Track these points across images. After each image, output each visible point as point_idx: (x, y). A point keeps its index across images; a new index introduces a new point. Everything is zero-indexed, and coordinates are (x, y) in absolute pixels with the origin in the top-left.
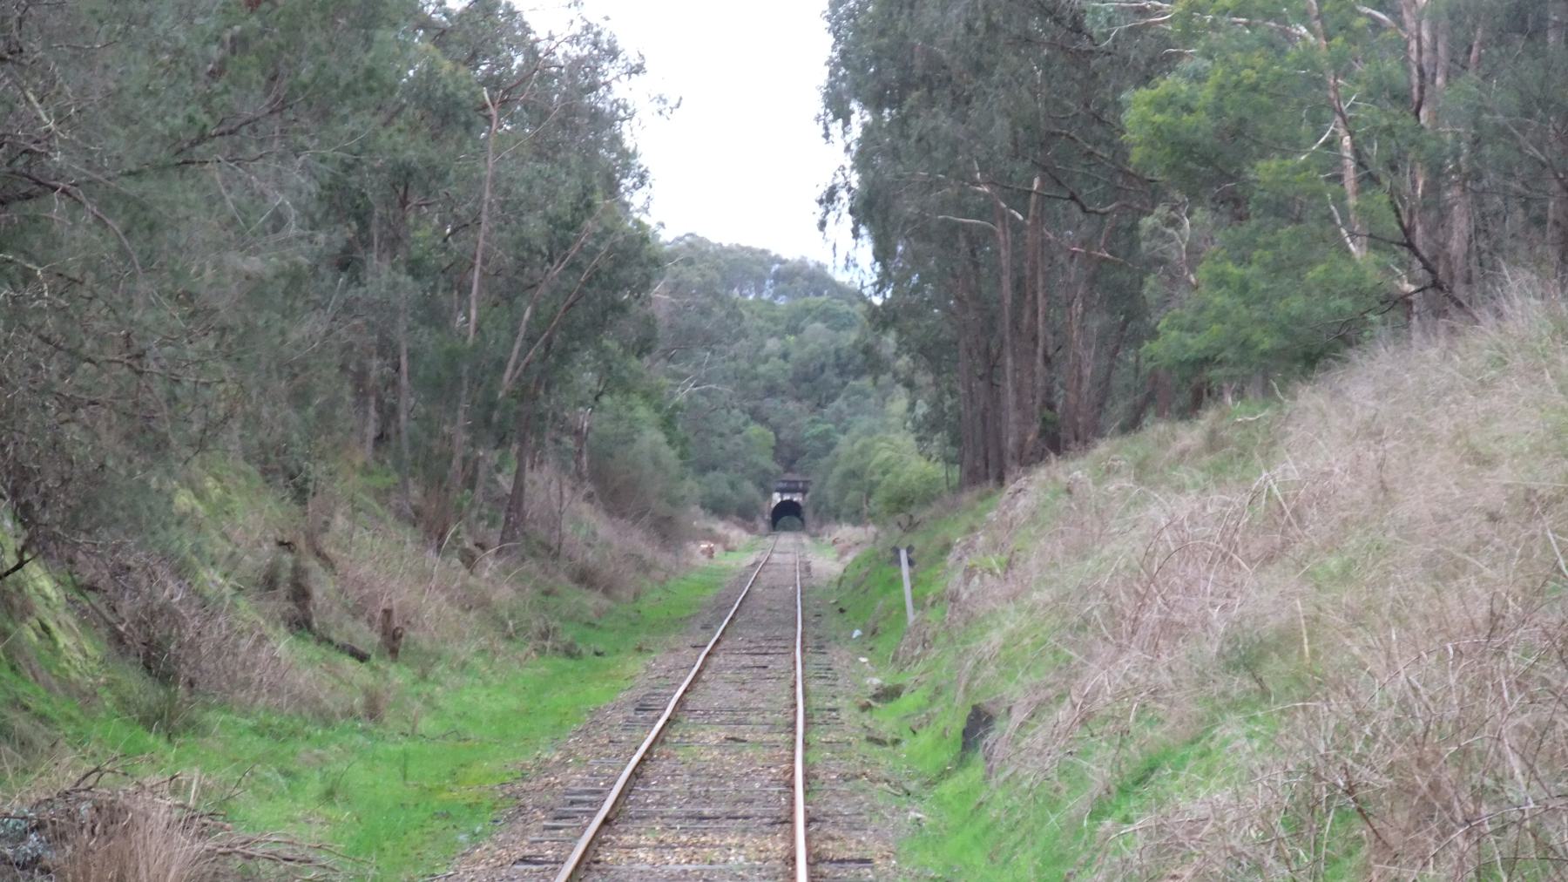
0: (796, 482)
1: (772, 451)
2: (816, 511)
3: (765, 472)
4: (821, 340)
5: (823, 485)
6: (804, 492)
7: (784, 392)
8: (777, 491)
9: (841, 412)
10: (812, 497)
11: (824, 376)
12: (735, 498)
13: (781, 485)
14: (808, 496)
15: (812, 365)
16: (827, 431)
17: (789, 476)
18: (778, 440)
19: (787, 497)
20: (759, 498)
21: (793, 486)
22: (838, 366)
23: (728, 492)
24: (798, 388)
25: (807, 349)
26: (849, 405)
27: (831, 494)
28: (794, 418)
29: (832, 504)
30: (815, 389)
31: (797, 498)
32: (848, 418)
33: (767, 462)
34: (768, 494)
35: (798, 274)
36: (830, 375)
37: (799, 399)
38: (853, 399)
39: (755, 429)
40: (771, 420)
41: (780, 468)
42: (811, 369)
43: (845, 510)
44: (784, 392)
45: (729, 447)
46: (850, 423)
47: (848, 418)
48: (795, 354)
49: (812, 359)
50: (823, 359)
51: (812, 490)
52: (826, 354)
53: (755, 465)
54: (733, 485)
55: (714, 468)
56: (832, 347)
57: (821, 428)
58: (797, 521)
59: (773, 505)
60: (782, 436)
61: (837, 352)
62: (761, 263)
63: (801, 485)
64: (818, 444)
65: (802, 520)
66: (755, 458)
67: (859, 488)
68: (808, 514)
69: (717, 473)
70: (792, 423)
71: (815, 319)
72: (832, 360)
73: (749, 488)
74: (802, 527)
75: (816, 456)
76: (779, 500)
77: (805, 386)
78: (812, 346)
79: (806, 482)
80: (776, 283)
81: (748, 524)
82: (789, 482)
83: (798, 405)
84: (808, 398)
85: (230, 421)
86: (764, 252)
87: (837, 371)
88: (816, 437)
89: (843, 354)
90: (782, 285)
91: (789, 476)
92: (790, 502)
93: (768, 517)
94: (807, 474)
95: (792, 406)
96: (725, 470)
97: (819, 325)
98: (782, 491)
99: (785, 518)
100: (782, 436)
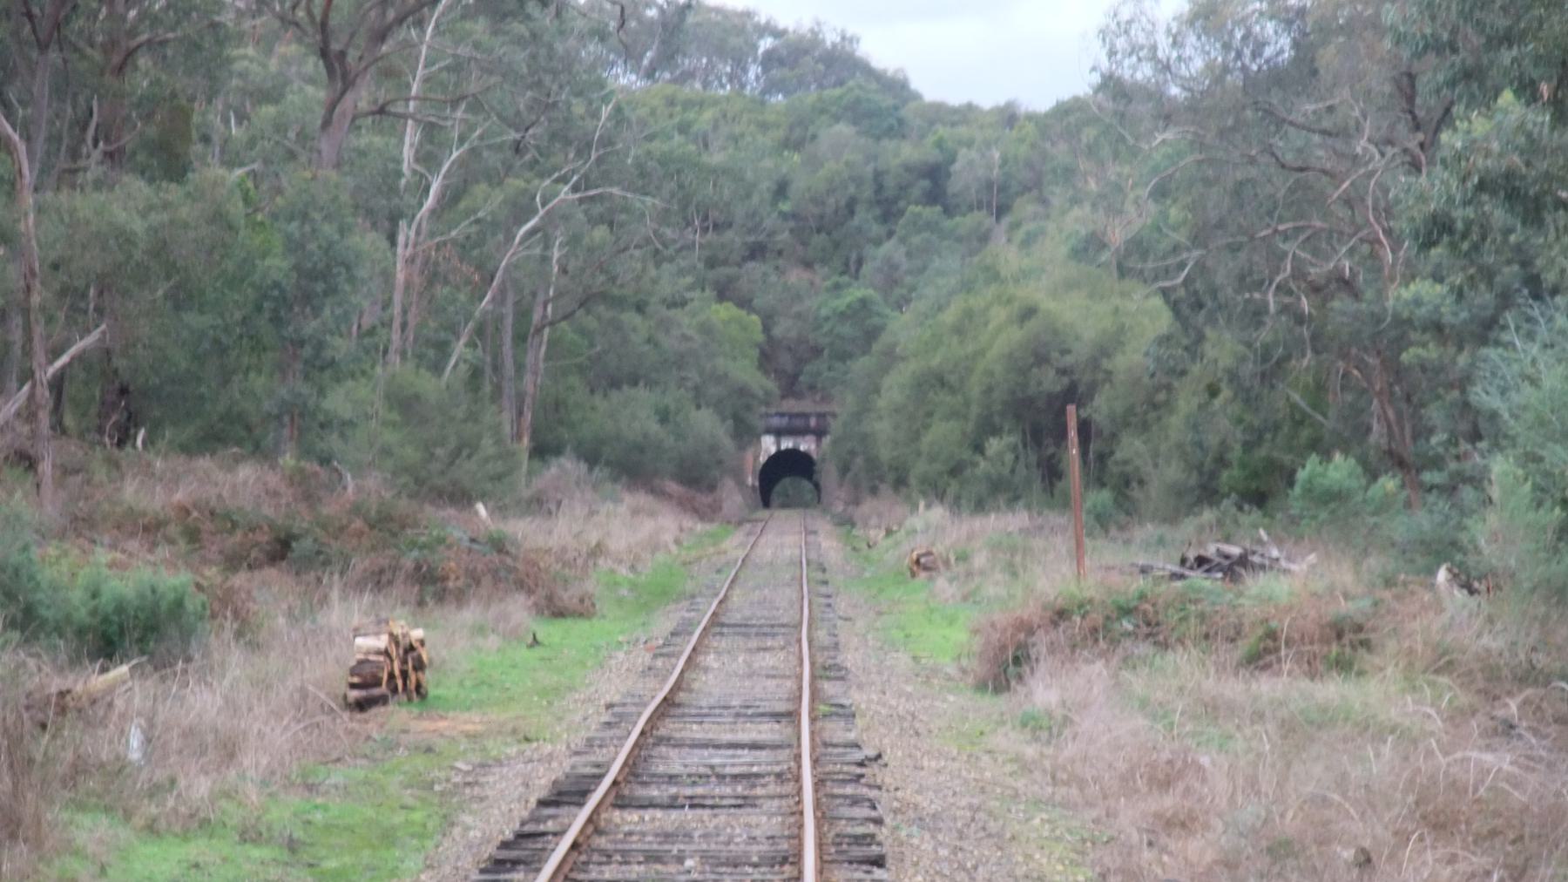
0: (806, 416)
1: (755, 353)
2: (845, 469)
3: (743, 391)
4: (847, 156)
5: (864, 409)
6: (819, 433)
7: (780, 253)
8: (768, 431)
9: (894, 267)
10: (834, 443)
11: (856, 221)
12: (670, 441)
13: (776, 422)
14: (827, 440)
15: (832, 200)
16: (864, 302)
17: (791, 405)
18: (770, 339)
19: (787, 444)
20: (728, 443)
21: (798, 423)
22: (879, 202)
23: (654, 427)
24: (805, 244)
25: (822, 173)
26: (909, 255)
27: (882, 427)
28: (798, 297)
29: (885, 454)
30: (837, 245)
31: (806, 445)
32: (908, 279)
33: (745, 372)
34: (745, 434)
35: (806, 52)
36: (864, 217)
37: (808, 265)
38: (916, 240)
39: (724, 312)
40: (757, 302)
41: (771, 384)
42: (829, 211)
43: (920, 468)
44: (780, 253)
45: (669, 343)
46: (913, 289)
47: (908, 279)
48: (799, 185)
49: (831, 191)
50: (852, 190)
51: (835, 426)
52: (858, 181)
53: (721, 379)
54: (664, 417)
55: (634, 382)
56: (869, 169)
57: (855, 293)
58: (806, 485)
59: (763, 459)
60: (777, 331)
61: (878, 175)
62: (740, 31)
63: (813, 422)
64: (846, 329)
65: (817, 486)
66: (721, 363)
67: (954, 414)
68: (829, 475)
69: (641, 393)
70: (796, 309)
71: (837, 119)
72: (868, 192)
73: (707, 424)
74: (817, 498)
75: (844, 357)
76: (773, 450)
77: (819, 240)
78: (831, 166)
79: (821, 416)
80: (766, 69)
81: (704, 499)
82: (792, 416)
83: (806, 275)
84: (824, 261)
85: (1468, 474)
86: (748, 15)
87: (878, 211)
88: (843, 316)
89: (890, 183)
90: (776, 73)
91: (791, 405)
92: (794, 454)
93: (751, 480)
94: (826, 399)
95: (796, 276)
96: (651, 384)
97: (844, 129)
98: (779, 433)
99: (786, 482)
100: (777, 331)
